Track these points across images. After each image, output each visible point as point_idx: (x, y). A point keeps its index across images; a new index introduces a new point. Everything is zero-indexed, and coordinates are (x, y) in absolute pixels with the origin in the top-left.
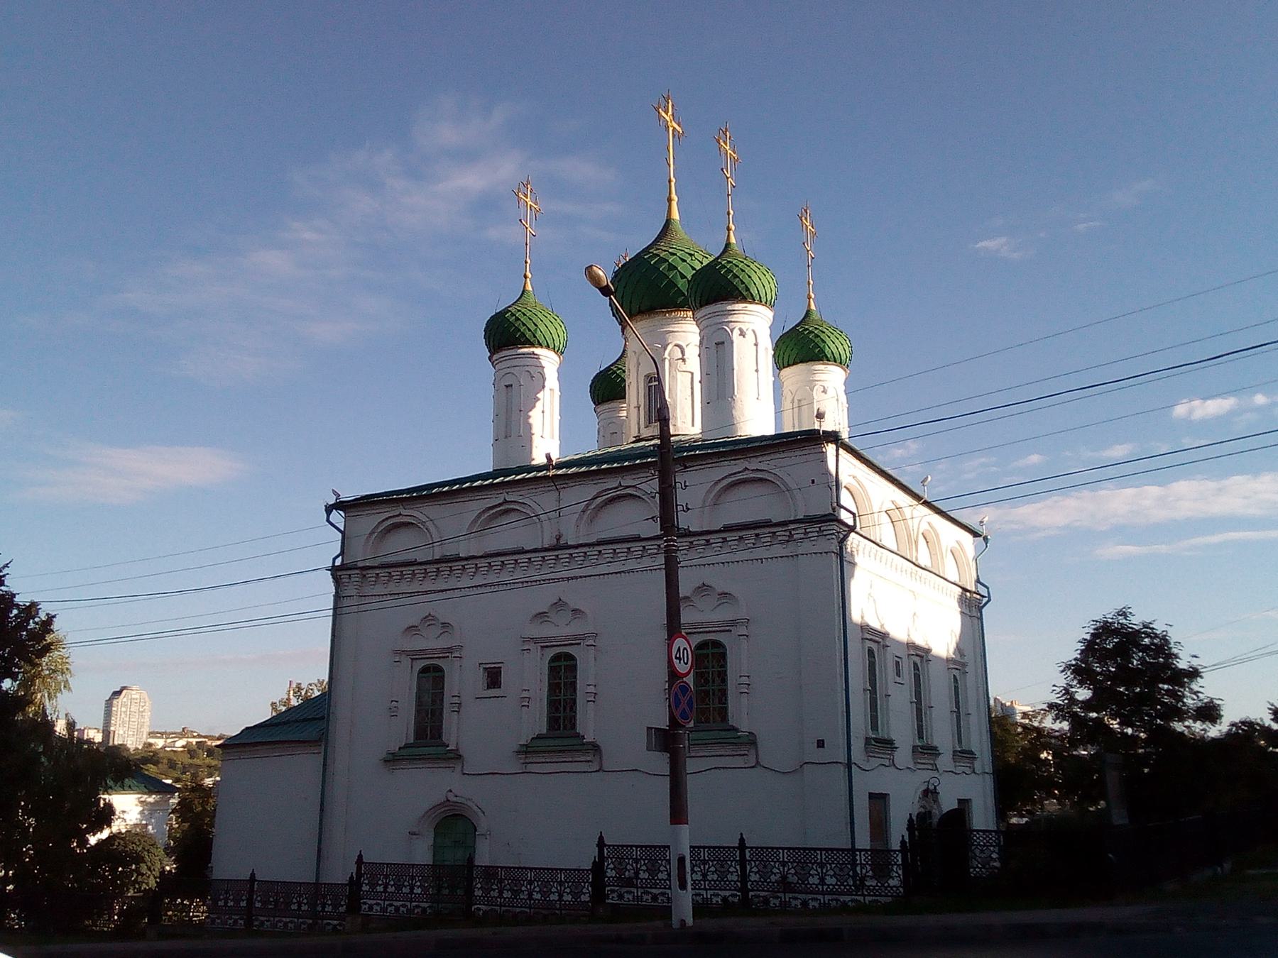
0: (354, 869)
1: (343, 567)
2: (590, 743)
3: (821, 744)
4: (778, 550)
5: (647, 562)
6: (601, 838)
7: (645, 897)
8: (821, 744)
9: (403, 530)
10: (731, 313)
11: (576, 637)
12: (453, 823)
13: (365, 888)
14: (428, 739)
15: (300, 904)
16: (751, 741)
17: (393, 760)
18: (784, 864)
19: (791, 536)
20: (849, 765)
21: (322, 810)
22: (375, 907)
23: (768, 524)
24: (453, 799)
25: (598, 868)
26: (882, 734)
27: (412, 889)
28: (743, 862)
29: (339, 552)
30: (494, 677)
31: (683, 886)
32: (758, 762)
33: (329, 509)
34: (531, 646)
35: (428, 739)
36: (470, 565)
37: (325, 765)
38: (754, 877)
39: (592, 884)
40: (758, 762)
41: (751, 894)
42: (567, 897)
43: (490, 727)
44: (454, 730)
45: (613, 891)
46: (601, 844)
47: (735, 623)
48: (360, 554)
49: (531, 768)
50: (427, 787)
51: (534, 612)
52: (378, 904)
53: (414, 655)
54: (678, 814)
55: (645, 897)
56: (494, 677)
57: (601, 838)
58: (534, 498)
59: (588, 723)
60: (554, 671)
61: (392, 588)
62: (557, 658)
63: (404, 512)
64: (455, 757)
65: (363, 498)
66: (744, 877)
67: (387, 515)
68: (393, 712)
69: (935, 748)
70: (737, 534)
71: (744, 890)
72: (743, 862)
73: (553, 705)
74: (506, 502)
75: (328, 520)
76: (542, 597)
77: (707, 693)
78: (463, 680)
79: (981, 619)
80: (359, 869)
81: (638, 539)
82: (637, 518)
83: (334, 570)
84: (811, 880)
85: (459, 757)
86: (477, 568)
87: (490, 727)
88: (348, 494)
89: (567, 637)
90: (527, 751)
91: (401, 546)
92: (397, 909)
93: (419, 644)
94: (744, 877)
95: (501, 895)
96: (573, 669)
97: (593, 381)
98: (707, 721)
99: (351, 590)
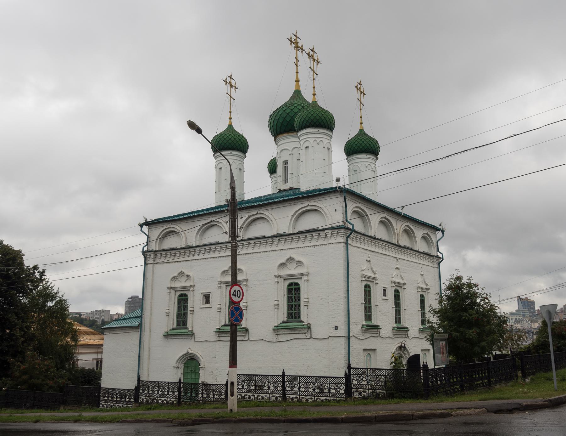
0: (136, 383)
1: (148, 251)
2: (244, 328)
4: (321, 242)
5: (222, 254)
9: (315, 212)
12: (191, 363)
13: (141, 391)
14: (181, 324)
16: (308, 328)
17: (167, 335)
19: (326, 235)
20: (349, 338)
21: (139, 356)
23: (316, 230)
24: (190, 352)
26: (374, 322)
28: (284, 382)
30: (207, 298)
31: (232, 395)
32: (311, 337)
33: (141, 226)
34: (222, 285)
35: (181, 324)
36: (197, 249)
37: (140, 337)
38: (288, 389)
40: (311, 337)
41: (353, 390)
42: (216, 396)
44: (193, 322)
47: (303, 274)
48: (154, 246)
49: (222, 339)
50: (180, 347)
52: (253, 395)
53: (176, 289)
54: (233, 363)
56: (207, 298)
58: (270, 212)
60: (289, 291)
61: (256, 250)
62: (291, 285)
63: (172, 226)
64: (191, 334)
66: (284, 388)
69: (406, 328)
71: (284, 394)
72: (284, 382)
73: (290, 307)
75: (141, 230)
77: (292, 305)
79: (439, 268)
82: (220, 234)
83: (144, 253)
84: (310, 390)
85: (193, 334)
86: (171, 254)
88: (150, 218)
91: (171, 242)
93: (177, 284)
94: (284, 388)
96: (186, 300)
98: (292, 318)
99: (150, 261)
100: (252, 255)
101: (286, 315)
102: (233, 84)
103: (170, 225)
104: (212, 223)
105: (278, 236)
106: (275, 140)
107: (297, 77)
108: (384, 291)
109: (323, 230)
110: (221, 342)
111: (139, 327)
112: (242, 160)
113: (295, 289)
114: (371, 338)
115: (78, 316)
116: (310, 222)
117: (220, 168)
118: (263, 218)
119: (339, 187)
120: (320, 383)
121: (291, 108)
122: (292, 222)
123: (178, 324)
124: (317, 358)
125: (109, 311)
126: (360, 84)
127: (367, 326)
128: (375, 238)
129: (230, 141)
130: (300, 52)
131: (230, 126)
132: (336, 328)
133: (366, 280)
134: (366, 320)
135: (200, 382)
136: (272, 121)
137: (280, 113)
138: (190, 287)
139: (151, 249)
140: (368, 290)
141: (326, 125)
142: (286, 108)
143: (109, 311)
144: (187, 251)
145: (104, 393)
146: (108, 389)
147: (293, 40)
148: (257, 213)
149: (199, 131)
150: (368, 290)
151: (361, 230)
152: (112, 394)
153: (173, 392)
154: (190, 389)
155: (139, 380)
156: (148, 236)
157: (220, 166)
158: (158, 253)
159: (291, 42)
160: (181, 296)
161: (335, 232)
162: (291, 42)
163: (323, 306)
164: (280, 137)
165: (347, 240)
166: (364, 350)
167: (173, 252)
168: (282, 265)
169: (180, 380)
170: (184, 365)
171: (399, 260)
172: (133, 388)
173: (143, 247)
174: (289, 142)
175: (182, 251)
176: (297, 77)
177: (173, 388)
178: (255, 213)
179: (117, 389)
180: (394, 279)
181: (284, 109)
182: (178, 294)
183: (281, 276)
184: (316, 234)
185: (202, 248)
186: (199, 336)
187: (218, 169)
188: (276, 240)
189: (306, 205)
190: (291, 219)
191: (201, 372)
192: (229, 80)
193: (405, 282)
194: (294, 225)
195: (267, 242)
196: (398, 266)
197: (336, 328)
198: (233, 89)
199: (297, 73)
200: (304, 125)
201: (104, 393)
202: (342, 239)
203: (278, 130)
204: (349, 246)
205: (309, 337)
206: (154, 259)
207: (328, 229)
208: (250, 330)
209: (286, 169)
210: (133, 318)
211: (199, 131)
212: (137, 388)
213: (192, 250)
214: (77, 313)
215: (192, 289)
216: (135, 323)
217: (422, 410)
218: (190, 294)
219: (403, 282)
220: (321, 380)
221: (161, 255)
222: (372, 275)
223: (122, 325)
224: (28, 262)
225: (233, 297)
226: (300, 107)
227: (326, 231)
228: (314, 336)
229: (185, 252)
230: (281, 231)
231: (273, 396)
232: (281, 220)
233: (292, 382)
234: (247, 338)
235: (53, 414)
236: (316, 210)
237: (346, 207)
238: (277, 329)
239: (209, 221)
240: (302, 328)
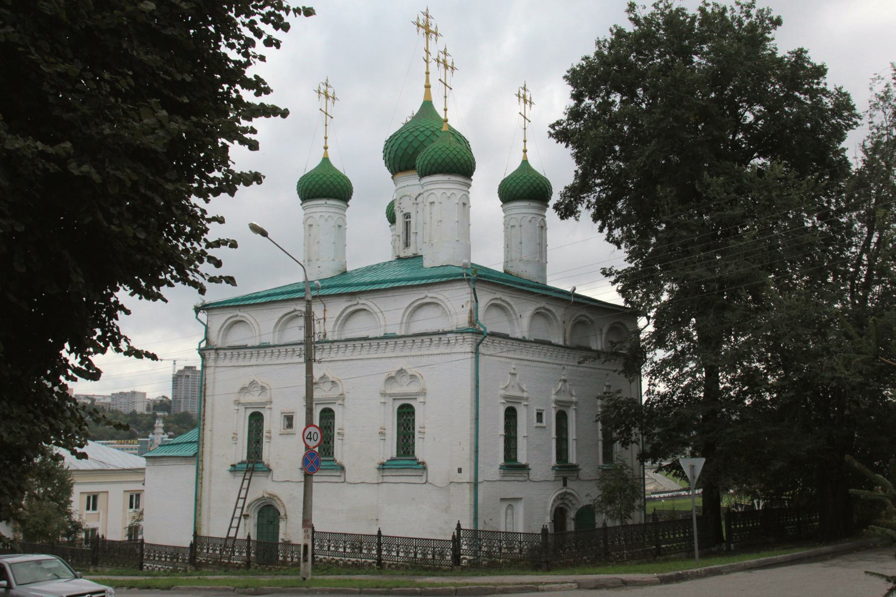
0: (192, 539)
4: (442, 349)
6: (459, 525)
9: (361, 313)
16: (342, 468)
18: (520, 542)
20: (475, 484)
25: (456, 540)
27: (345, 549)
28: (379, 544)
29: (203, 338)
36: (276, 350)
38: (384, 553)
39: (452, 549)
44: (269, 452)
45: (465, 558)
49: (386, 479)
51: (240, 386)
53: (247, 406)
57: (459, 525)
58: (374, 301)
59: (421, 451)
63: (240, 314)
67: (231, 315)
68: (235, 437)
70: (353, 343)
72: (379, 544)
74: (295, 310)
76: (393, 367)
78: (272, 423)
80: (459, 533)
81: (245, 347)
85: (425, 468)
89: (329, 399)
90: (383, 467)
91: (238, 337)
94: (379, 551)
95: (398, 555)
100: (351, 362)
101: (395, 450)
102: (330, 94)
103: (236, 312)
105: (386, 337)
107: (427, 80)
108: (539, 415)
110: (385, 485)
112: (342, 212)
113: (409, 413)
115: (89, 402)
116: (428, 321)
117: (311, 226)
118: (365, 310)
121: (415, 134)
122: (411, 309)
124: (420, 514)
125: (144, 394)
126: (525, 89)
129: (324, 186)
130: (433, 39)
131: (326, 160)
132: (460, 471)
135: (280, 541)
136: (388, 151)
137: (399, 142)
138: (266, 403)
140: (511, 415)
142: (408, 133)
143: (144, 394)
144: (262, 351)
145: (149, 551)
146: (154, 545)
147: (421, 23)
149: (264, 234)
152: (160, 553)
153: (241, 553)
154: (265, 550)
155: (195, 535)
156: (206, 326)
157: (310, 222)
158: (221, 352)
159: (419, 25)
160: (402, 407)
162: (419, 25)
163: (443, 439)
164: (400, 176)
165: (477, 349)
166: (502, 499)
167: (242, 351)
168: (390, 379)
169: (249, 537)
170: (259, 512)
172: (188, 545)
173: (200, 343)
174: (411, 182)
175: (254, 351)
176: (427, 80)
179: (166, 547)
181: (404, 135)
183: (390, 395)
185: (283, 349)
187: (307, 227)
188: (383, 343)
190: (404, 315)
191: (282, 525)
192: (323, 88)
194: (408, 323)
195: (371, 345)
197: (460, 471)
198: (330, 102)
199: (427, 73)
200: (428, 170)
201: (149, 551)
202: (468, 348)
203: (397, 166)
204: (481, 358)
206: (216, 359)
207: (451, 332)
208: (347, 468)
209: (407, 224)
210: (186, 443)
211: (264, 234)
212: (193, 546)
214: (87, 397)
215: (268, 406)
217: (478, 584)
218: (266, 414)
220: (425, 543)
221: (225, 354)
223: (171, 454)
226: (428, 133)
227: (449, 335)
229: (258, 353)
230: (390, 330)
232: (389, 313)
233: (389, 545)
235: (279, 578)
237: (477, 301)
239: (292, 309)
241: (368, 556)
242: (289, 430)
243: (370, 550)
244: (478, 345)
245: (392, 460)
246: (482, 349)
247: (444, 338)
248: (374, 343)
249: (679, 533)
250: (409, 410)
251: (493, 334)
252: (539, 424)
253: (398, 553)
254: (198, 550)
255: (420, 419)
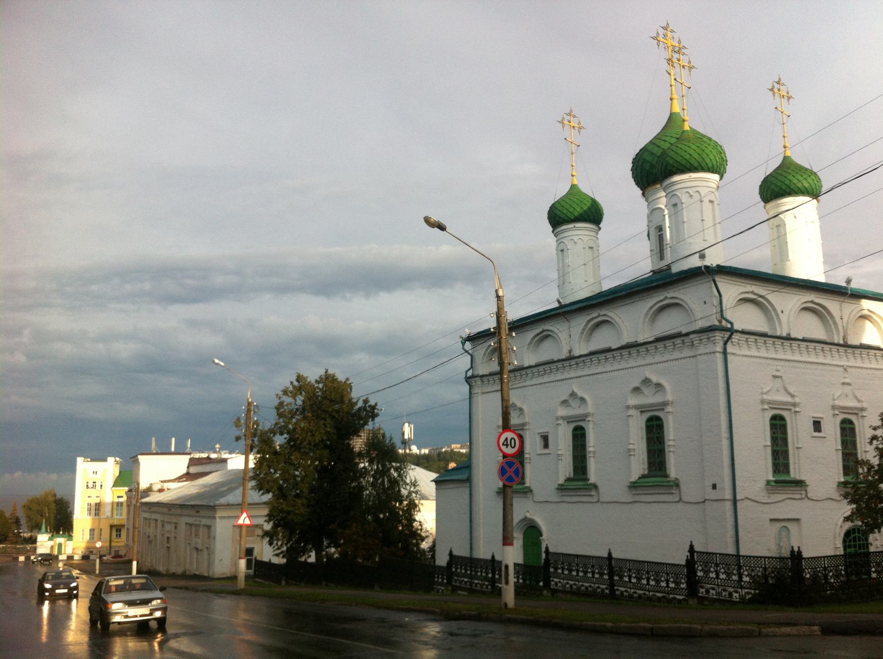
1: (473, 377)
2: (591, 484)
3: (714, 487)
4: (687, 352)
5: (490, 388)
6: (692, 547)
7: (724, 593)
8: (714, 487)
10: (674, 184)
11: (658, 404)
13: (700, 574)
15: (667, 581)
16: (677, 484)
22: (712, 592)
23: (679, 335)
26: (794, 474)
30: (817, 425)
32: (681, 499)
33: (463, 344)
37: (471, 494)
43: (546, 470)
46: (692, 550)
49: (637, 498)
53: (642, 409)
55: (724, 593)
56: (817, 425)
57: (692, 547)
65: (479, 333)
74: (666, 298)
75: (463, 349)
77: (777, 438)
78: (799, 432)
85: (531, 491)
87: (546, 470)
92: (571, 586)
97: (761, 187)
101: (646, 466)
104: (545, 333)
106: (643, 194)
109: (687, 334)
110: (637, 504)
111: (468, 480)
114: (788, 501)
117: (562, 251)
119: (707, 267)
120: (655, 569)
123: (651, 465)
127: (776, 482)
128: (788, 338)
133: (771, 408)
134: (846, 474)
139: (476, 373)
140: (778, 425)
141: (703, 165)
144: (517, 374)
148: (599, 316)
149: (442, 228)
150: (778, 425)
151: (763, 327)
160: (650, 420)
161: (704, 336)
165: (725, 348)
166: (771, 520)
171: (849, 370)
173: (467, 372)
177: (601, 567)
178: (595, 315)
180: (837, 403)
182: (646, 416)
184: (678, 341)
186: (539, 495)
189: (662, 297)
193: (865, 405)
196: (847, 381)
204: (729, 356)
205: (677, 499)
211: (442, 228)
213: (523, 372)
216: (462, 476)
219: (859, 405)
222: (788, 399)
224: (357, 394)
225: (504, 448)
227: (692, 336)
228: (684, 499)
231: (725, 590)
234: (595, 499)
236: (677, 304)
238: (634, 486)
240: (667, 486)
241: (600, 581)
242: (546, 451)
243: (601, 574)
244: (725, 343)
245: (643, 476)
246: (730, 348)
247: (686, 339)
248: (616, 353)
249: (461, 569)
250: (658, 422)
251: (743, 332)
252: (817, 434)
253: (717, 575)
254: (552, 570)
255: (671, 433)
